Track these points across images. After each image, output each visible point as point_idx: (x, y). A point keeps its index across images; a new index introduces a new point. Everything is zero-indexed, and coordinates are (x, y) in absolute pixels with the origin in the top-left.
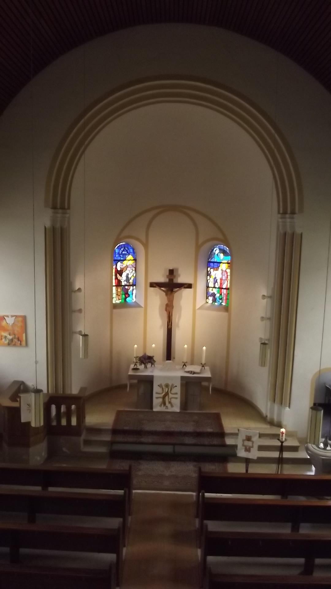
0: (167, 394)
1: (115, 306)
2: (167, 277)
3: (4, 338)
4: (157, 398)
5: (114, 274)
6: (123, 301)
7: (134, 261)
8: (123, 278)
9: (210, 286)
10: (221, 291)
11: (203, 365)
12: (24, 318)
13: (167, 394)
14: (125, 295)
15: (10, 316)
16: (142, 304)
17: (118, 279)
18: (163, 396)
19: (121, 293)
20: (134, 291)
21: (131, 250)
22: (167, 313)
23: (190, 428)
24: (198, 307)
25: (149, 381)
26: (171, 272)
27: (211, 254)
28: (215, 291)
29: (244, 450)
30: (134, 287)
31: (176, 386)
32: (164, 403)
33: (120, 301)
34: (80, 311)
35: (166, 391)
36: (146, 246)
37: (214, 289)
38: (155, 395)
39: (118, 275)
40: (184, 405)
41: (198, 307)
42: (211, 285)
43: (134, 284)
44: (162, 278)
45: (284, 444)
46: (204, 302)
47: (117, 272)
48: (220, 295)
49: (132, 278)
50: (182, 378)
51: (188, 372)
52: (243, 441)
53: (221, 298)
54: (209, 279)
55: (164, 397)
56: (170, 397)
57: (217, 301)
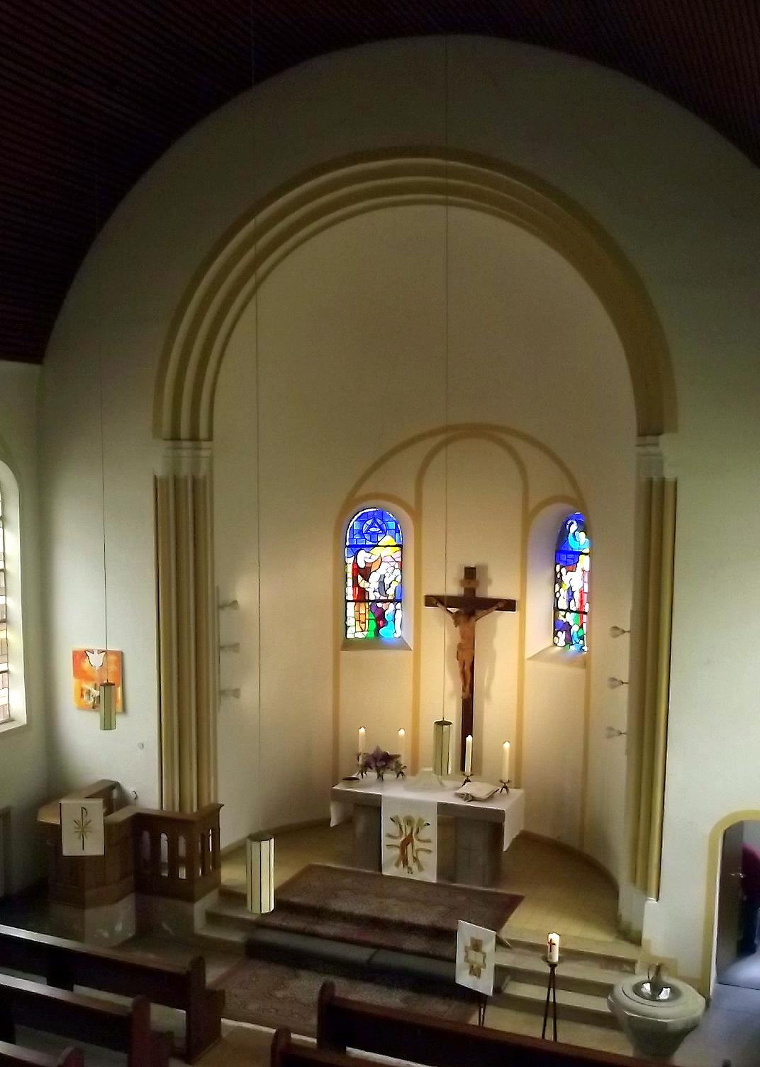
0: (408, 840)
1: (349, 644)
2: (462, 583)
3: (86, 693)
4: (389, 846)
5: (350, 575)
6: (372, 635)
7: (398, 548)
8: (371, 586)
12: (120, 656)
13: (408, 840)
14: (376, 622)
15: (96, 652)
16: (411, 644)
17: (359, 586)
18: (402, 842)
19: (367, 617)
22: (458, 666)
24: (528, 654)
26: (470, 573)
27: (563, 534)
28: (570, 618)
29: (468, 971)
30: (399, 606)
31: (428, 824)
32: (406, 862)
33: (365, 633)
35: (408, 832)
36: (416, 514)
38: (385, 841)
39: (360, 578)
42: (562, 604)
44: (454, 590)
45: (558, 971)
47: (357, 570)
48: (580, 628)
49: (393, 586)
50: (442, 807)
51: (461, 796)
53: (580, 634)
54: (559, 592)
55: (403, 847)
56: (415, 848)
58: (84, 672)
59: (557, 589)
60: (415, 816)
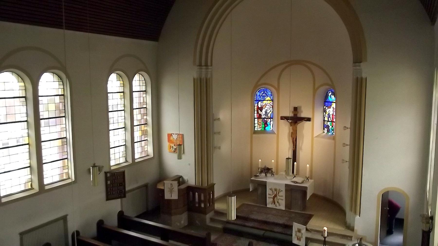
0: (275, 196)
2: (293, 112)
9: (325, 120)
10: (333, 124)
11: (307, 178)
12: (183, 135)
13: (275, 196)
16: (276, 132)
20: (272, 122)
21: (270, 93)
23: (281, 221)
24: (315, 136)
25: (264, 185)
26: (296, 109)
27: (327, 96)
28: (329, 123)
30: (272, 120)
31: (282, 191)
32: (274, 203)
34: (219, 133)
36: (278, 90)
37: (328, 122)
38: (268, 196)
39: (259, 111)
40: (288, 205)
41: (315, 136)
42: (326, 119)
43: (272, 117)
44: (289, 113)
46: (323, 132)
47: (258, 108)
50: (286, 185)
52: (296, 232)
54: (325, 115)
55: (274, 198)
57: (330, 132)
58: (171, 140)
59: (325, 114)
60: (278, 188)
